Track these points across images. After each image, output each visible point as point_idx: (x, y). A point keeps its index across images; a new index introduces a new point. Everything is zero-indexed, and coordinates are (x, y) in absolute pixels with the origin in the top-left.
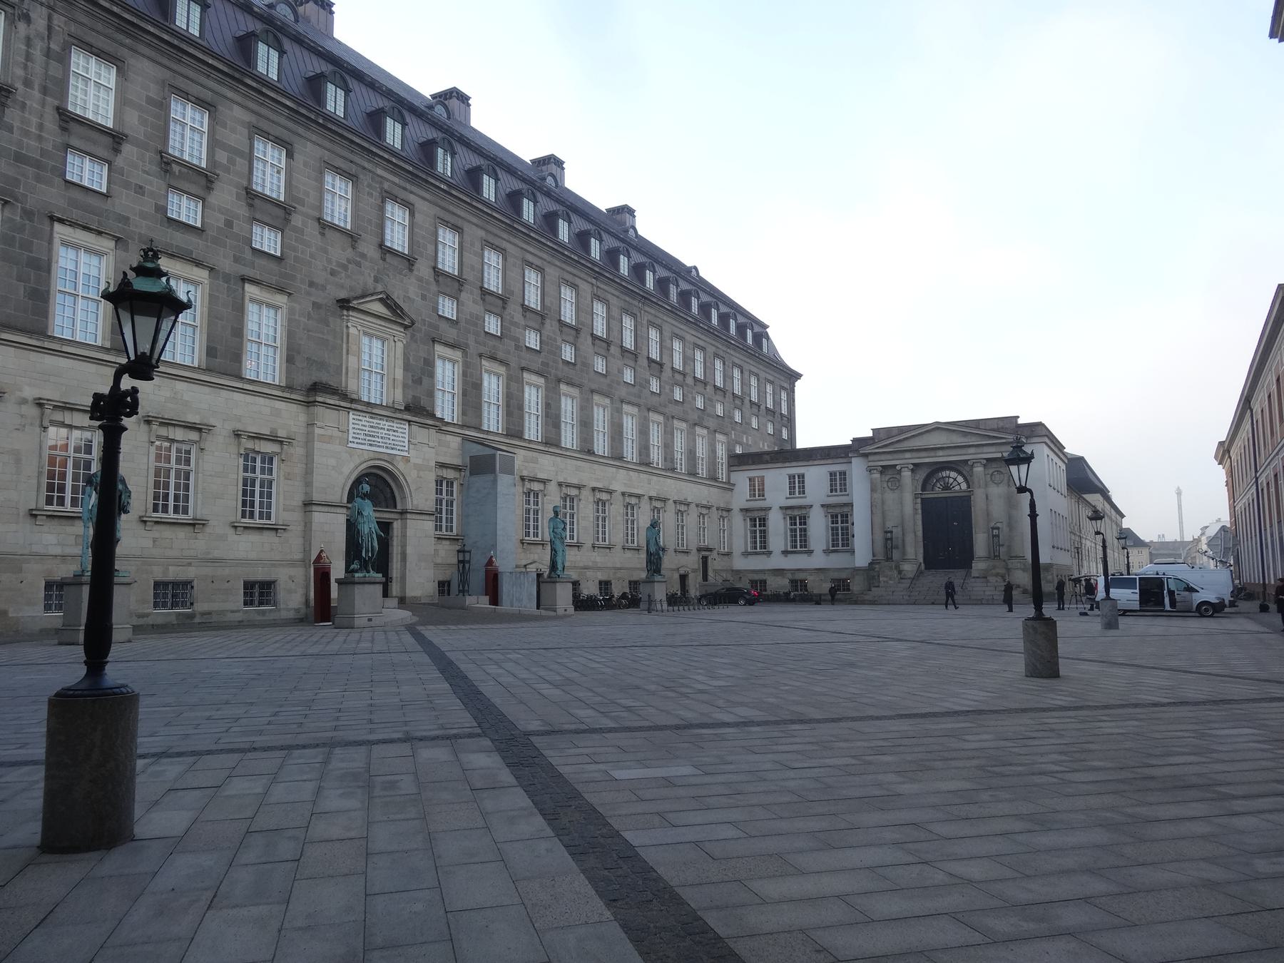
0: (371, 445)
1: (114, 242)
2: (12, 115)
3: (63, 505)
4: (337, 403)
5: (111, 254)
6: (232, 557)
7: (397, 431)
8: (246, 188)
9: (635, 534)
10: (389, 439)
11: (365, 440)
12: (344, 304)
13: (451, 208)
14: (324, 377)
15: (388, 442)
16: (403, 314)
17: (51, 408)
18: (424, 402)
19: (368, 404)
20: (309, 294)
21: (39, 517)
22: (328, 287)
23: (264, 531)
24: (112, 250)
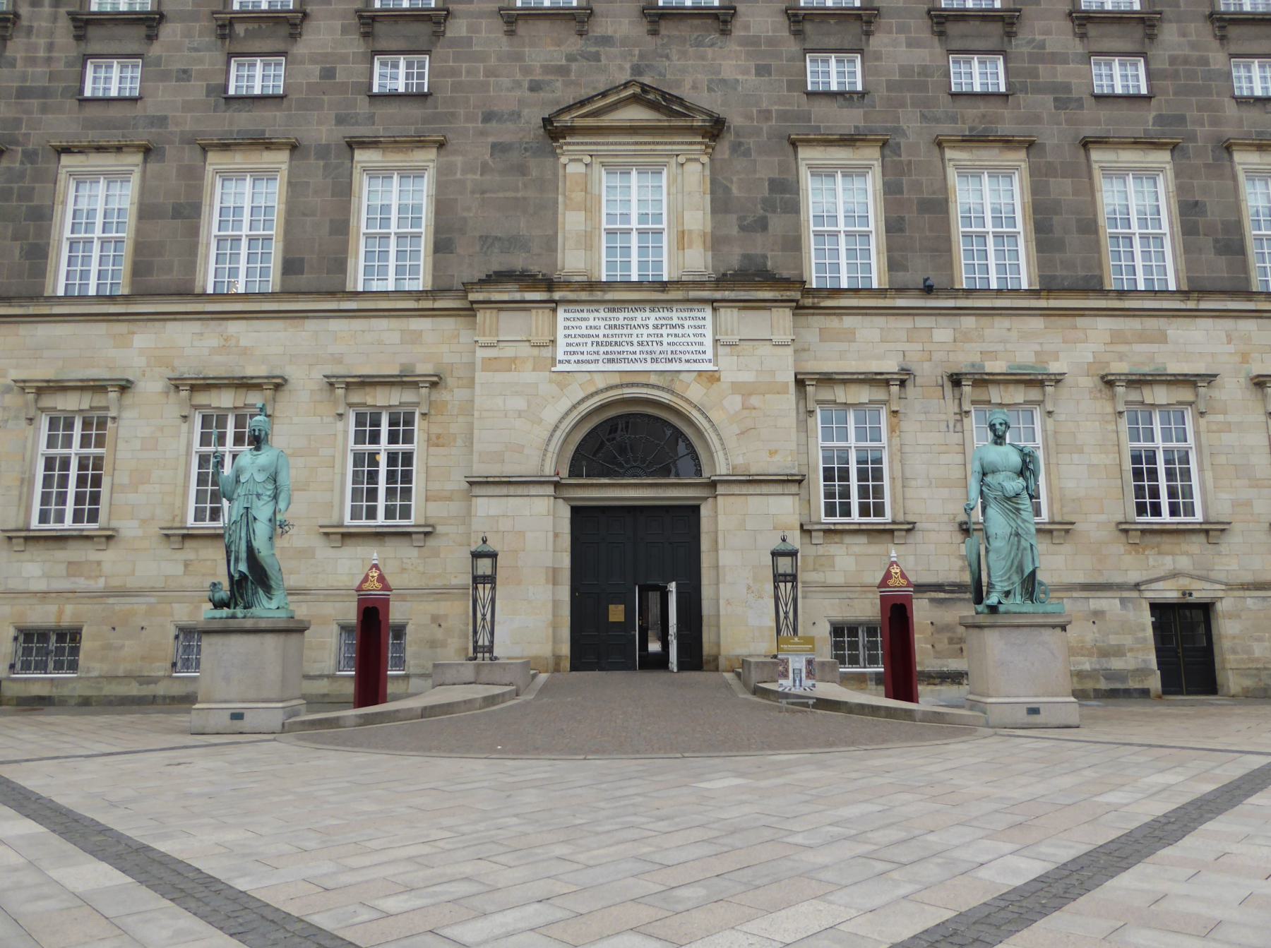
0: (611, 361)
1: (878, 149)
2: (16, 47)
3: (1160, 515)
4: (518, 296)
5: (876, 165)
6: (323, 585)
8: (1211, 15)
11: (598, 353)
12: (554, 131)
16: (687, 108)
17: (814, 383)
18: (776, 262)
20: (483, 133)
21: (414, 536)
22: (526, 112)
23: (387, 539)
24: (1024, 161)
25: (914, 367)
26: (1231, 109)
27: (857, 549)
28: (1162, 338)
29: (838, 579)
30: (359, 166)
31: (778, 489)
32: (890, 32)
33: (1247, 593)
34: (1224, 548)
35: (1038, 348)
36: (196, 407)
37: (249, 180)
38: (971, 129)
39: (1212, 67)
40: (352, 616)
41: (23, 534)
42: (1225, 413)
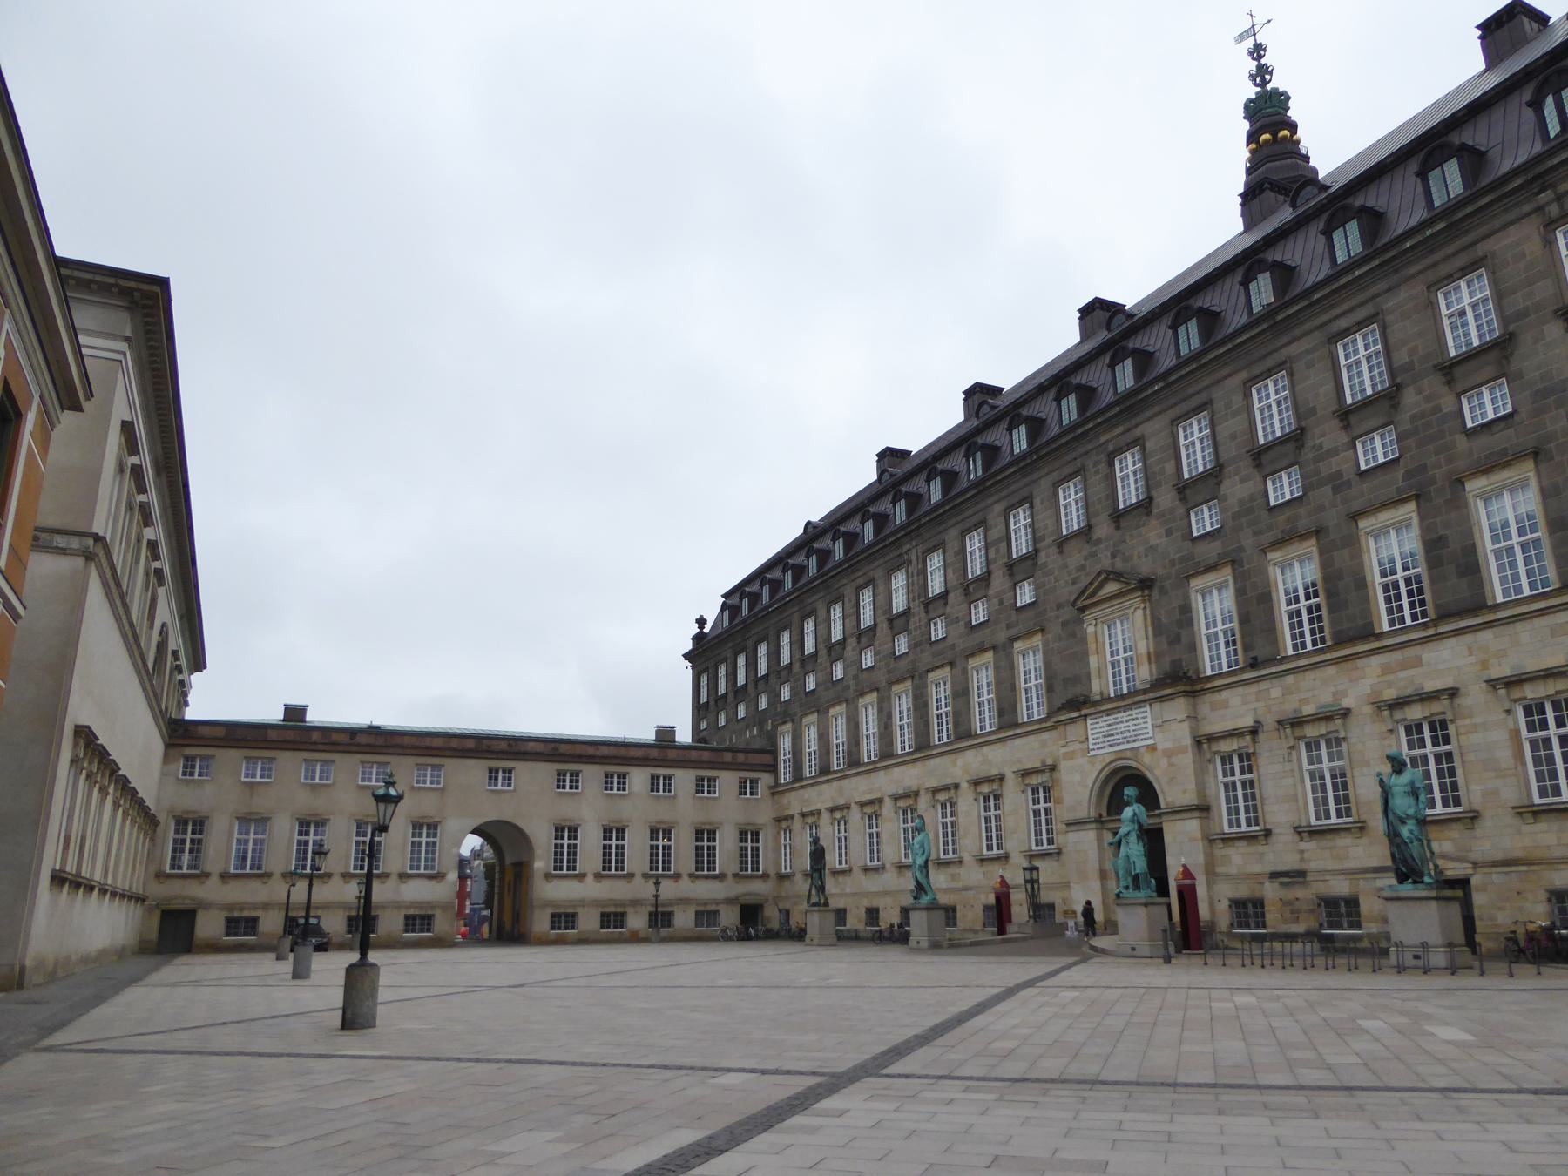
0: (1111, 746)
7: (1137, 719)
9: (941, 836)
10: (1129, 731)
13: (1191, 390)
14: (1078, 690)
15: (1128, 734)
19: (1121, 697)
20: (1057, 617)
25: (1261, 719)
26: (1462, 443)
27: (1241, 850)
28: (1418, 662)
29: (1234, 870)
30: (1471, 495)
31: (1189, 815)
32: (1230, 477)
33: (1494, 869)
34: (1478, 832)
35: (1333, 689)
36: (1398, 722)
37: (1506, 495)
38: (1282, 532)
39: (1445, 411)
40: (991, 899)
41: (1530, 809)
42: (1471, 717)
